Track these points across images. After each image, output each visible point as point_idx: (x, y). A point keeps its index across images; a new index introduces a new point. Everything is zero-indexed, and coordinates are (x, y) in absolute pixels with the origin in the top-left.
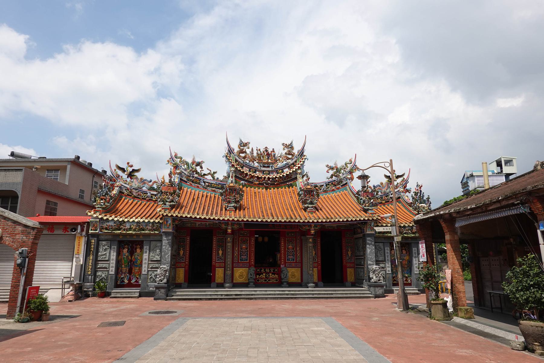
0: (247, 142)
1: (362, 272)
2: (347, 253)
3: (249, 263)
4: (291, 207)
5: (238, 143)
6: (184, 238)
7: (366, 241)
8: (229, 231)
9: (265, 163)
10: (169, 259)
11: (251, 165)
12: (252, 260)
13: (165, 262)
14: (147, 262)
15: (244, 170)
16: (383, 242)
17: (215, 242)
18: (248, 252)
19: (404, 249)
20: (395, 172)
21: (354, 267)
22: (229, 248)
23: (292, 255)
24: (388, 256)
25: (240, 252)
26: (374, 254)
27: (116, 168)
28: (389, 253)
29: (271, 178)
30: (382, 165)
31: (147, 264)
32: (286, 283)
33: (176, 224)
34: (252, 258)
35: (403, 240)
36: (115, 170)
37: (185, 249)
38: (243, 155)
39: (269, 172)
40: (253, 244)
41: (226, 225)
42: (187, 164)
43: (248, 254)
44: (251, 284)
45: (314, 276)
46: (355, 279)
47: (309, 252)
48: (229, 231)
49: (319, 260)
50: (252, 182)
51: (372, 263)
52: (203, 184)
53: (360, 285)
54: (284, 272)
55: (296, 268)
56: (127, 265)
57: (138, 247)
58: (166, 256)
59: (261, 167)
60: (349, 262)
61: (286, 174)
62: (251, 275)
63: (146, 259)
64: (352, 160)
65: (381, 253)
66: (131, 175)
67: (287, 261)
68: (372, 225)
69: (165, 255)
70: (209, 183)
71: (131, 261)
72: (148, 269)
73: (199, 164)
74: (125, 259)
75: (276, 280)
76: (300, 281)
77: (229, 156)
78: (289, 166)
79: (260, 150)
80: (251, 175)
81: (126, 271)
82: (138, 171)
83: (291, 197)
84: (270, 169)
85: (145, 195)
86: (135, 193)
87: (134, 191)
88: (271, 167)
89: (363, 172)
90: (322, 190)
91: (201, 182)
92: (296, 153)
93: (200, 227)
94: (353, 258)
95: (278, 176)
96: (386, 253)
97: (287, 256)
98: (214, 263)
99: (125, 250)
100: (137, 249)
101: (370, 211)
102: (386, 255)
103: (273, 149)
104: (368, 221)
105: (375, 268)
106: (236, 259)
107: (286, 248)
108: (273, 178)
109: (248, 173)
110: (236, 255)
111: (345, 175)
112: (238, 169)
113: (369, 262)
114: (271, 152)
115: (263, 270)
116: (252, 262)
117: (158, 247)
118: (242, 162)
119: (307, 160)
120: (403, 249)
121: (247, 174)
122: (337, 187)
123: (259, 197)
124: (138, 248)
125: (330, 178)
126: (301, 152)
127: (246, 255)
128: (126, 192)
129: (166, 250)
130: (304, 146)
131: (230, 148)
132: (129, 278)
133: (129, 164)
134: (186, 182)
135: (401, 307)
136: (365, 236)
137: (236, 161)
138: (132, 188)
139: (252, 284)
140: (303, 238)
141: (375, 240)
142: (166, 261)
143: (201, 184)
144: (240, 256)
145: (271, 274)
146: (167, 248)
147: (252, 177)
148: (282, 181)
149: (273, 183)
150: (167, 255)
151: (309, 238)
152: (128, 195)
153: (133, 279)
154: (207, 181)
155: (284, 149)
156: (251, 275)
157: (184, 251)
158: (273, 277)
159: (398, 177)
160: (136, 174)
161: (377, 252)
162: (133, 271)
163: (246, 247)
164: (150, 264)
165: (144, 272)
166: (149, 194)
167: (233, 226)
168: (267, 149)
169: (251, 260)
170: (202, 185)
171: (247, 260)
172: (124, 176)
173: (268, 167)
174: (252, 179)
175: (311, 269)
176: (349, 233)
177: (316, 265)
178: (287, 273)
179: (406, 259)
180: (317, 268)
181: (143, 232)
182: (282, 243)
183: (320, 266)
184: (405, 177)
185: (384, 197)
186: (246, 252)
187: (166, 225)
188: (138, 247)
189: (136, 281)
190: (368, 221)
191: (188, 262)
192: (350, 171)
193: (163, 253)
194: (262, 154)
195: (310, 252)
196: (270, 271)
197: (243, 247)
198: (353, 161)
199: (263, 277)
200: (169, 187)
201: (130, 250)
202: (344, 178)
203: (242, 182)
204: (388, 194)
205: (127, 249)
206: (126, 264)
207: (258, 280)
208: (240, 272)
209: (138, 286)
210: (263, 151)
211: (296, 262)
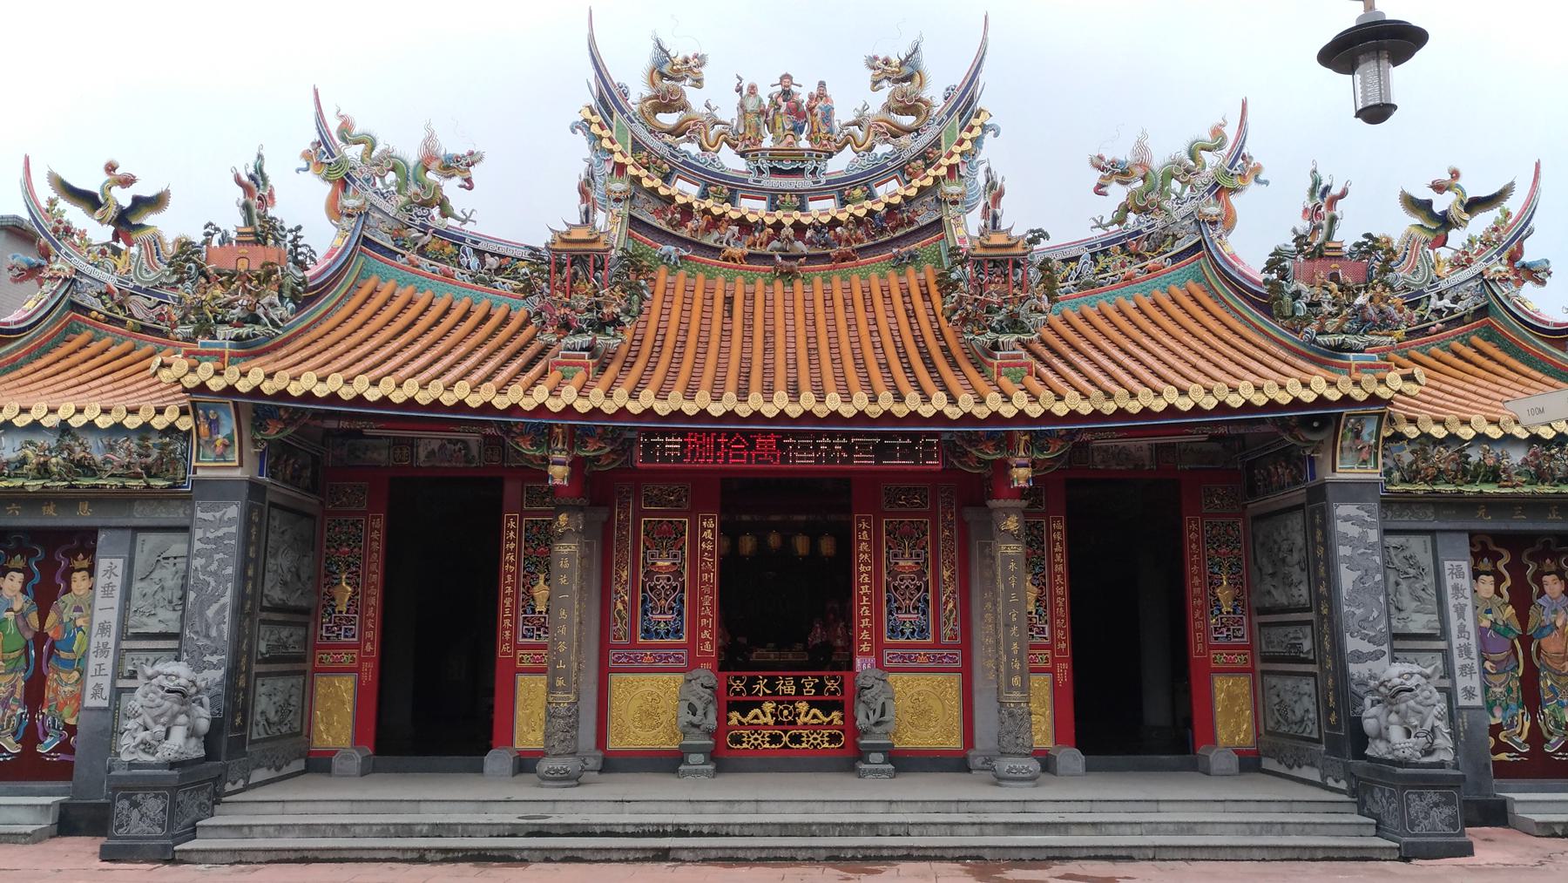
0: (691, 56)
1: (1306, 699)
3: (691, 646)
4: (903, 355)
5: (644, 59)
8: (559, 473)
10: (226, 628)
11: (710, 168)
13: (202, 642)
14: (112, 645)
15: (673, 191)
16: (1431, 532)
17: (514, 541)
18: (682, 591)
19: (1554, 568)
20: (1460, 182)
21: (1252, 671)
22: (563, 571)
24: (1461, 611)
27: (54, 196)
29: (808, 227)
31: (111, 653)
32: (879, 757)
33: (269, 442)
34: (704, 621)
35: (1302, 593)
37: (358, 576)
38: (668, 119)
40: (712, 552)
41: (538, 445)
43: (682, 601)
44: (693, 758)
46: (1258, 735)
47: (1002, 587)
48: (559, 473)
49: (1060, 634)
50: (715, 251)
51: (1371, 648)
52: (474, 262)
53: (1290, 767)
54: (868, 695)
55: (940, 677)
56: (18, 659)
57: (77, 565)
58: (210, 613)
59: (761, 172)
61: (888, 205)
62: (694, 714)
63: (104, 628)
64: (1226, 130)
65: (1423, 594)
66: (125, 222)
68: (1365, 434)
69: (203, 605)
70: (501, 256)
71: (40, 637)
72: (113, 682)
73: (451, 166)
74: (11, 628)
75: (834, 739)
76: (955, 743)
77: (600, 125)
78: (903, 171)
79: (753, 90)
80: (706, 211)
81: (12, 693)
82: (156, 202)
83: (911, 314)
86: (140, 308)
87: (141, 300)
88: (813, 173)
91: (464, 252)
92: (939, 102)
93: (438, 464)
95: (843, 217)
96: (1450, 591)
97: (890, 613)
98: (506, 647)
100: (76, 575)
101: (1351, 355)
102: (1451, 602)
103: (822, 84)
104: (1348, 406)
107: (885, 571)
108: (818, 228)
109: (695, 205)
110: (620, 606)
111: (1188, 207)
112: (646, 183)
113: (1352, 644)
115: (760, 686)
117: (172, 561)
118: (665, 151)
119: (996, 135)
120: (1546, 570)
121: (687, 210)
122: (1150, 263)
123: (748, 318)
125: (1112, 224)
128: (101, 308)
129: (211, 580)
130: (981, 61)
132: (26, 729)
133: (118, 172)
134: (393, 254)
136: (1324, 497)
137: (637, 146)
138: (131, 285)
139: (700, 758)
140: (970, 514)
142: (207, 636)
143: (464, 261)
145: (802, 707)
146: (213, 567)
147: (716, 221)
148: (867, 242)
149: (820, 251)
150: (215, 607)
152: (110, 320)
153: (46, 734)
154: (492, 248)
155: (876, 84)
156: (694, 714)
157: (355, 586)
158: (815, 721)
159: (1475, 205)
160: (150, 219)
161: (1397, 584)
162: (49, 694)
163: (674, 564)
164: (128, 656)
165: (94, 696)
167: (580, 448)
168: (793, 88)
169: (702, 629)
170: (469, 268)
171: (677, 632)
172: (101, 233)
173: (798, 172)
174: (716, 235)
175: (1016, 681)
176: (1220, 491)
180: (1049, 676)
181: (91, 481)
182: (864, 546)
183: (1065, 666)
184: (1514, 204)
186: (675, 589)
187: (212, 442)
188: (77, 565)
190: (1346, 411)
191: (373, 645)
192: (1216, 184)
195: (1008, 588)
196: (799, 692)
198: (1231, 133)
199: (762, 720)
201: (36, 580)
205: (19, 577)
206: (13, 655)
207: (738, 740)
209: (62, 771)
211: (937, 645)
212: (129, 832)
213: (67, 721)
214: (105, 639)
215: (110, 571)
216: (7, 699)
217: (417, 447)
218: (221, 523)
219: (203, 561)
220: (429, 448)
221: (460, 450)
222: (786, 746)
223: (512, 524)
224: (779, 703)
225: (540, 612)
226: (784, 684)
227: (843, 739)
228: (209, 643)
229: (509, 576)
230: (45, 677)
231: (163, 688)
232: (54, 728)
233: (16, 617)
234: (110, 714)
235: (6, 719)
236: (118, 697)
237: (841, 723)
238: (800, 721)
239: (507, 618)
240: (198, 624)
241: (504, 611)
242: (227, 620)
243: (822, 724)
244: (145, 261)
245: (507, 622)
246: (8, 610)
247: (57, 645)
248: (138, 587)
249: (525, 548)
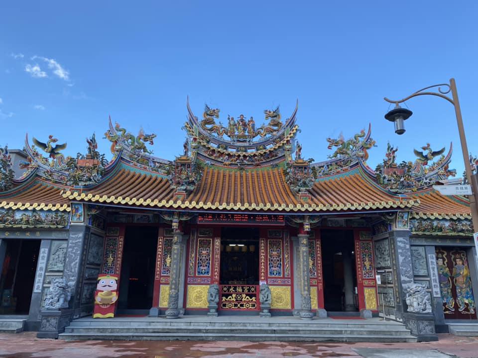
2: (364, 264)
3: (212, 277)
6: (115, 239)
7: (397, 244)
9: (238, 137)
10: (77, 269)
12: (216, 273)
16: (424, 246)
19: (459, 257)
23: (277, 266)
24: (433, 269)
25: (198, 260)
26: (411, 265)
27: (34, 144)
28: (435, 264)
30: (435, 90)
36: (33, 146)
38: (209, 126)
39: (246, 149)
40: (218, 249)
42: (131, 137)
43: (209, 264)
45: (312, 300)
46: (378, 306)
49: (319, 275)
51: (408, 279)
52: (152, 165)
58: (72, 264)
59: (234, 141)
60: (366, 278)
62: (212, 297)
66: (53, 153)
67: (269, 276)
69: (71, 262)
76: (289, 307)
79: (233, 119)
82: (63, 147)
84: (246, 144)
88: (249, 142)
89: (398, 105)
90: (321, 173)
94: (373, 271)
97: (270, 268)
98: (157, 277)
102: (431, 266)
103: (252, 118)
105: (416, 287)
106: (191, 271)
111: (354, 153)
114: (249, 121)
115: (232, 289)
116: (215, 276)
119: (300, 132)
125: (333, 157)
126: (290, 122)
127: (206, 265)
131: (191, 116)
135: (209, 217)
136: (393, 235)
139: (214, 310)
141: (410, 242)
142: (71, 272)
144: (199, 267)
145: (244, 296)
147: (222, 154)
148: (265, 161)
150: (74, 263)
151: (303, 237)
156: (212, 297)
159: (435, 154)
160: (60, 151)
164: (48, 277)
165: (37, 289)
169: (215, 272)
173: (245, 141)
175: (306, 288)
177: (314, 282)
178: (268, 295)
179: (463, 273)
180: (316, 287)
183: (321, 284)
184: (445, 153)
185: (415, 183)
186: (207, 260)
189: (467, 309)
194: (236, 125)
196: (243, 290)
197: (203, 252)
199: (232, 300)
200: (88, 160)
202: (353, 156)
203: (207, 162)
204: (421, 178)
207: (225, 305)
208: (197, 292)
210: (237, 121)
211: (284, 277)
214: (41, 272)
215: (44, 252)
218: (78, 238)
224: (237, 294)
231: (58, 286)
238: (243, 299)
243: (249, 301)
248: (52, 257)
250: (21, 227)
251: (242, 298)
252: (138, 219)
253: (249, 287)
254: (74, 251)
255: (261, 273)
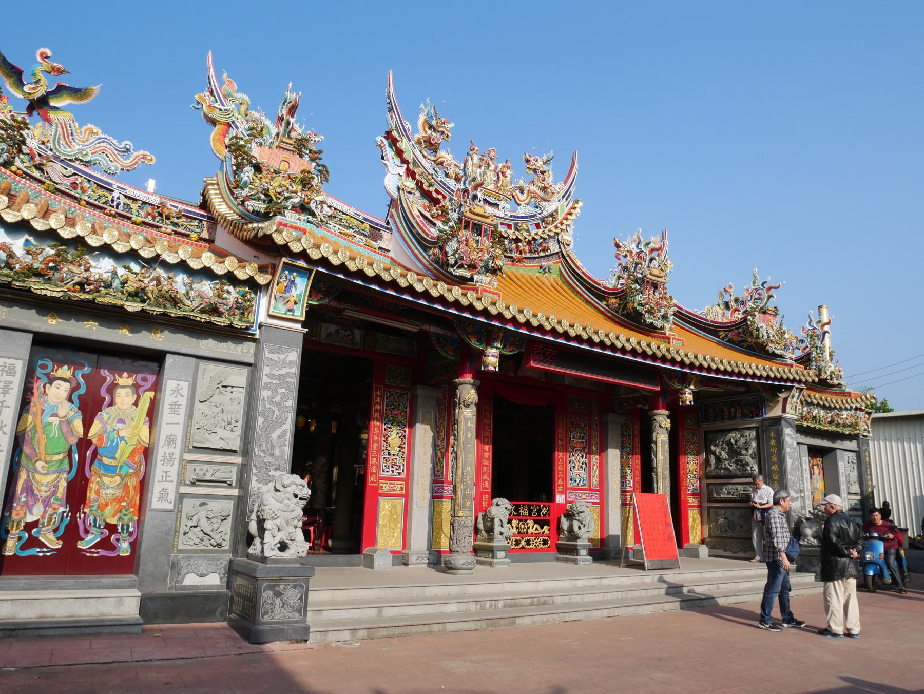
12: (485, 477)
13: (268, 459)
14: (177, 455)
23: (581, 467)
31: (177, 462)
56: (61, 461)
58: (275, 435)
63: (170, 440)
69: (270, 428)
71: (84, 443)
72: (178, 488)
85: (100, 192)
87: (58, 166)
93: (333, 343)
99: (58, 392)
124: (124, 387)
129: (276, 409)
142: (272, 455)
145: (531, 523)
153: (87, 532)
158: (537, 532)
162: (91, 495)
164: (190, 467)
165: (161, 499)
166: (116, 194)
173: (496, 205)
189: (105, 544)
193: (260, 421)
196: (530, 511)
201: (82, 390)
205: (66, 386)
209: (128, 565)
212: (273, 618)
213: (108, 521)
214: (171, 450)
215: (177, 391)
216: (49, 498)
217: (321, 328)
218: (284, 364)
219: (270, 393)
220: (329, 331)
221: (348, 335)
222: (523, 547)
223: (379, 393)
224: (520, 521)
225: (394, 455)
226: (523, 510)
227: (549, 542)
228: (273, 461)
229: (376, 428)
230: (88, 480)
231: (296, 496)
232: (95, 526)
233: (60, 422)
234: (174, 516)
235: (47, 517)
236: (181, 502)
237: (548, 532)
238: (530, 531)
239: (374, 457)
240: (264, 444)
241: (372, 452)
242: (287, 442)
243: (539, 533)
244: (62, 137)
245: (374, 460)
246: (53, 415)
247: (100, 451)
249: (386, 410)
250: (653, 323)
251: (528, 528)
252: (330, 334)
253: (539, 506)
254: (278, 399)
255: (559, 479)
